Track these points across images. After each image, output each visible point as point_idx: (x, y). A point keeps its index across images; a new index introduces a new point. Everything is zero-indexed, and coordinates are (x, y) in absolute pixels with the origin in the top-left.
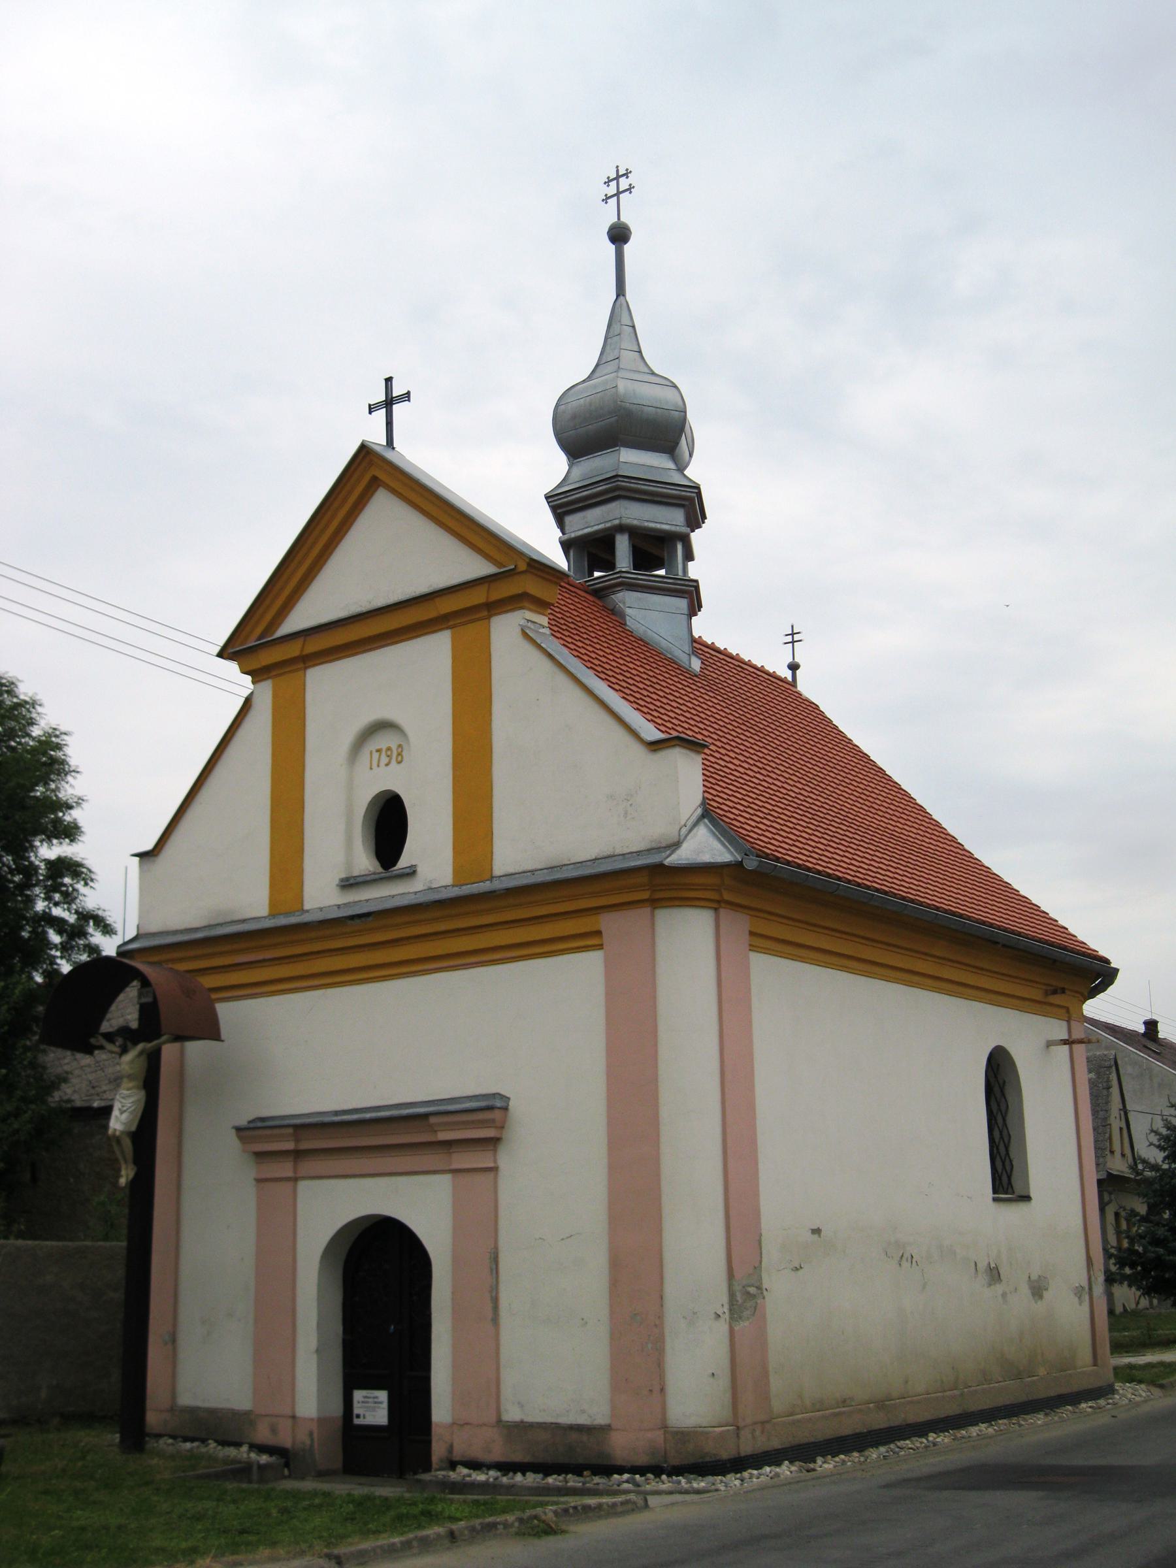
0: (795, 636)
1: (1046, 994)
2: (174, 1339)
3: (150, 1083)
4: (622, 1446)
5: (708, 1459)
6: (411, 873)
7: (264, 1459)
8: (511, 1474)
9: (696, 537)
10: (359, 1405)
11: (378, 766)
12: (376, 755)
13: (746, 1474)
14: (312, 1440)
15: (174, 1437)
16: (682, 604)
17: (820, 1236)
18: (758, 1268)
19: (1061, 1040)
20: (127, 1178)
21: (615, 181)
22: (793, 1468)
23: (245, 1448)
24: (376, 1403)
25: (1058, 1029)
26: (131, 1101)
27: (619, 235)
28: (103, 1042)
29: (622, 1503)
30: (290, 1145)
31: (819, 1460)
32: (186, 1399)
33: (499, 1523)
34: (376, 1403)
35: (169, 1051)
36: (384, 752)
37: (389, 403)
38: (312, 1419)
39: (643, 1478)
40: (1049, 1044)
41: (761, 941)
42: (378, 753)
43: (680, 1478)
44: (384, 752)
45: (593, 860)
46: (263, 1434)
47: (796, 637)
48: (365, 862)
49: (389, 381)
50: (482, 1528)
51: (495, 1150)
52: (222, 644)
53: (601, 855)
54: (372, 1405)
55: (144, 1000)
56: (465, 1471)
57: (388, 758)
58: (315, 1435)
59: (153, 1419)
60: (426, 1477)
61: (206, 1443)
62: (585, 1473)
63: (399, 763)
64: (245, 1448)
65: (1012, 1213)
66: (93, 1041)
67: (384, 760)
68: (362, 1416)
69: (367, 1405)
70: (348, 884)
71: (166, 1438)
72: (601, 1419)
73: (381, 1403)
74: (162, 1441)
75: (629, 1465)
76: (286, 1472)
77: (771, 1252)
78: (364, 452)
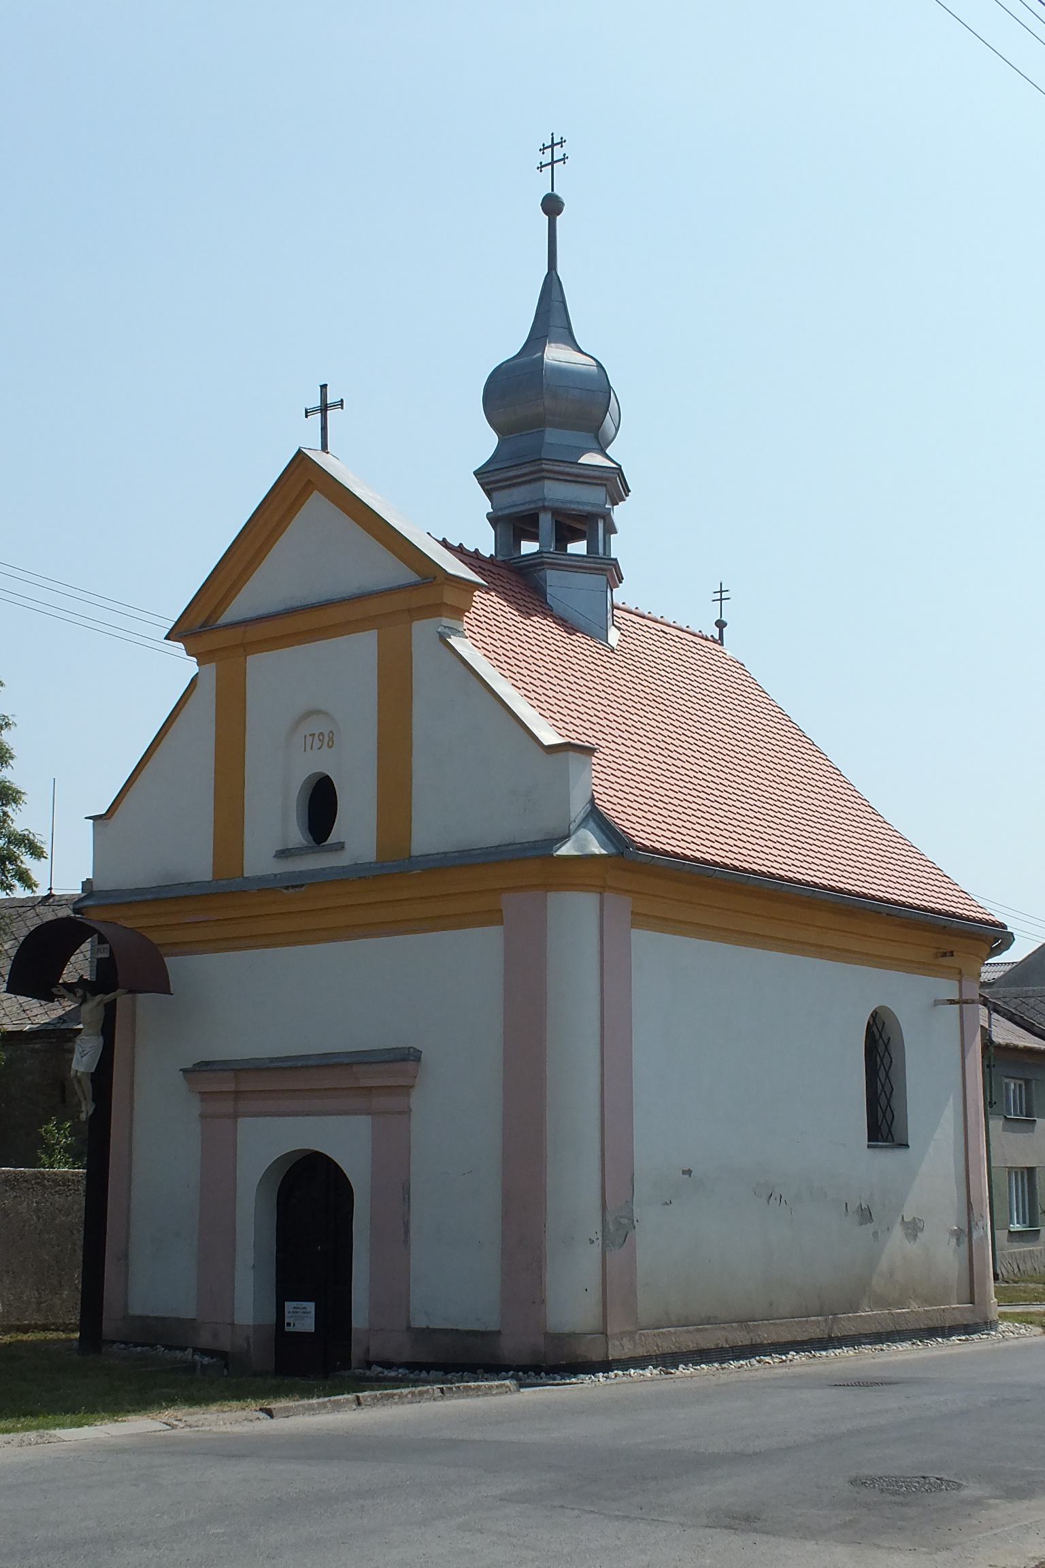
0: (719, 598)
1: (936, 956)
2: (125, 1256)
3: (108, 1031)
4: (509, 1348)
5: (580, 1360)
6: (340, 846)
7: (206, 1360)
8: (417, 1372)
9: (619, 513)
10: (290, 1315)
11: (312, 748)
12: (309, 739)
13: (612, 1374)
14: (248, 1344)
15: (126, 1343)
16: (600, 580)
17: (690, 1176)
18: (630, 1202)
19: (948, 1000)
20: (87, 1113)
21: (550, 149)
22: (655, 1372)
23: (190, 1351)
24: (304, 1312)
25: (947, 988)
26: (90, 1045)
27: (552, 206)
28: (63, 991)
29: (497, 1387)
30: (230, 1087)
31: (681, 1366)
32: (136, 1309)
33: (395, 1395)
34: (304, 1312)
35: (122, 1000)
36: (316, 737)
37: (324, 408)
38: (249, 1326)
39: (526, 1375)
40: (937, 1003)
41: (641, 920)
42: (311, 737)
43: (556, 1375)
44: (316, 737)
45: (496, 847)
46: (205, 1340)
47: (724, 595)
48: (297, 836)
49: (324, 387)
50: (381, 1397)
51: (409, 1095)
52: (170, 628)
53: (504, 843)
54: (301, 1315)
55: (100, 956)
56: (380, 1369)
57: (321, 743)
58: (251, 1340)
59: (109, 1326)
60: (347, 1373)
61: (155, 1348)
62: (478, 1371)
63: (331, 732)
64: (190, 1351)
65: (887, 1159)
66: (54, 990)
67: (317, 743)
68: (292, 1325)
69: (297, 1314)
70: (283, 854)
71: (118, 1344)
72: (493, 1327)
73: (310, 1312)
74: (115, 1346)
75: (515, 1364)
76: (226, 1372)
77: (642, 1189)
78: (300, 458)
